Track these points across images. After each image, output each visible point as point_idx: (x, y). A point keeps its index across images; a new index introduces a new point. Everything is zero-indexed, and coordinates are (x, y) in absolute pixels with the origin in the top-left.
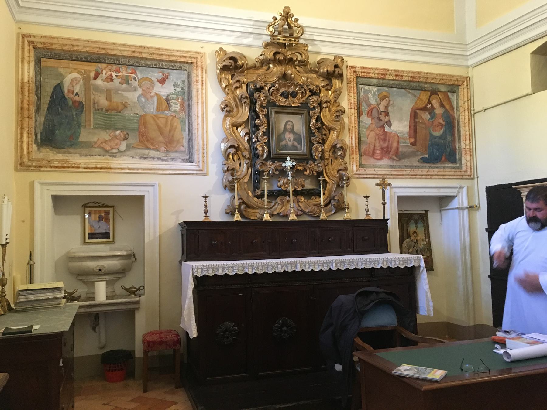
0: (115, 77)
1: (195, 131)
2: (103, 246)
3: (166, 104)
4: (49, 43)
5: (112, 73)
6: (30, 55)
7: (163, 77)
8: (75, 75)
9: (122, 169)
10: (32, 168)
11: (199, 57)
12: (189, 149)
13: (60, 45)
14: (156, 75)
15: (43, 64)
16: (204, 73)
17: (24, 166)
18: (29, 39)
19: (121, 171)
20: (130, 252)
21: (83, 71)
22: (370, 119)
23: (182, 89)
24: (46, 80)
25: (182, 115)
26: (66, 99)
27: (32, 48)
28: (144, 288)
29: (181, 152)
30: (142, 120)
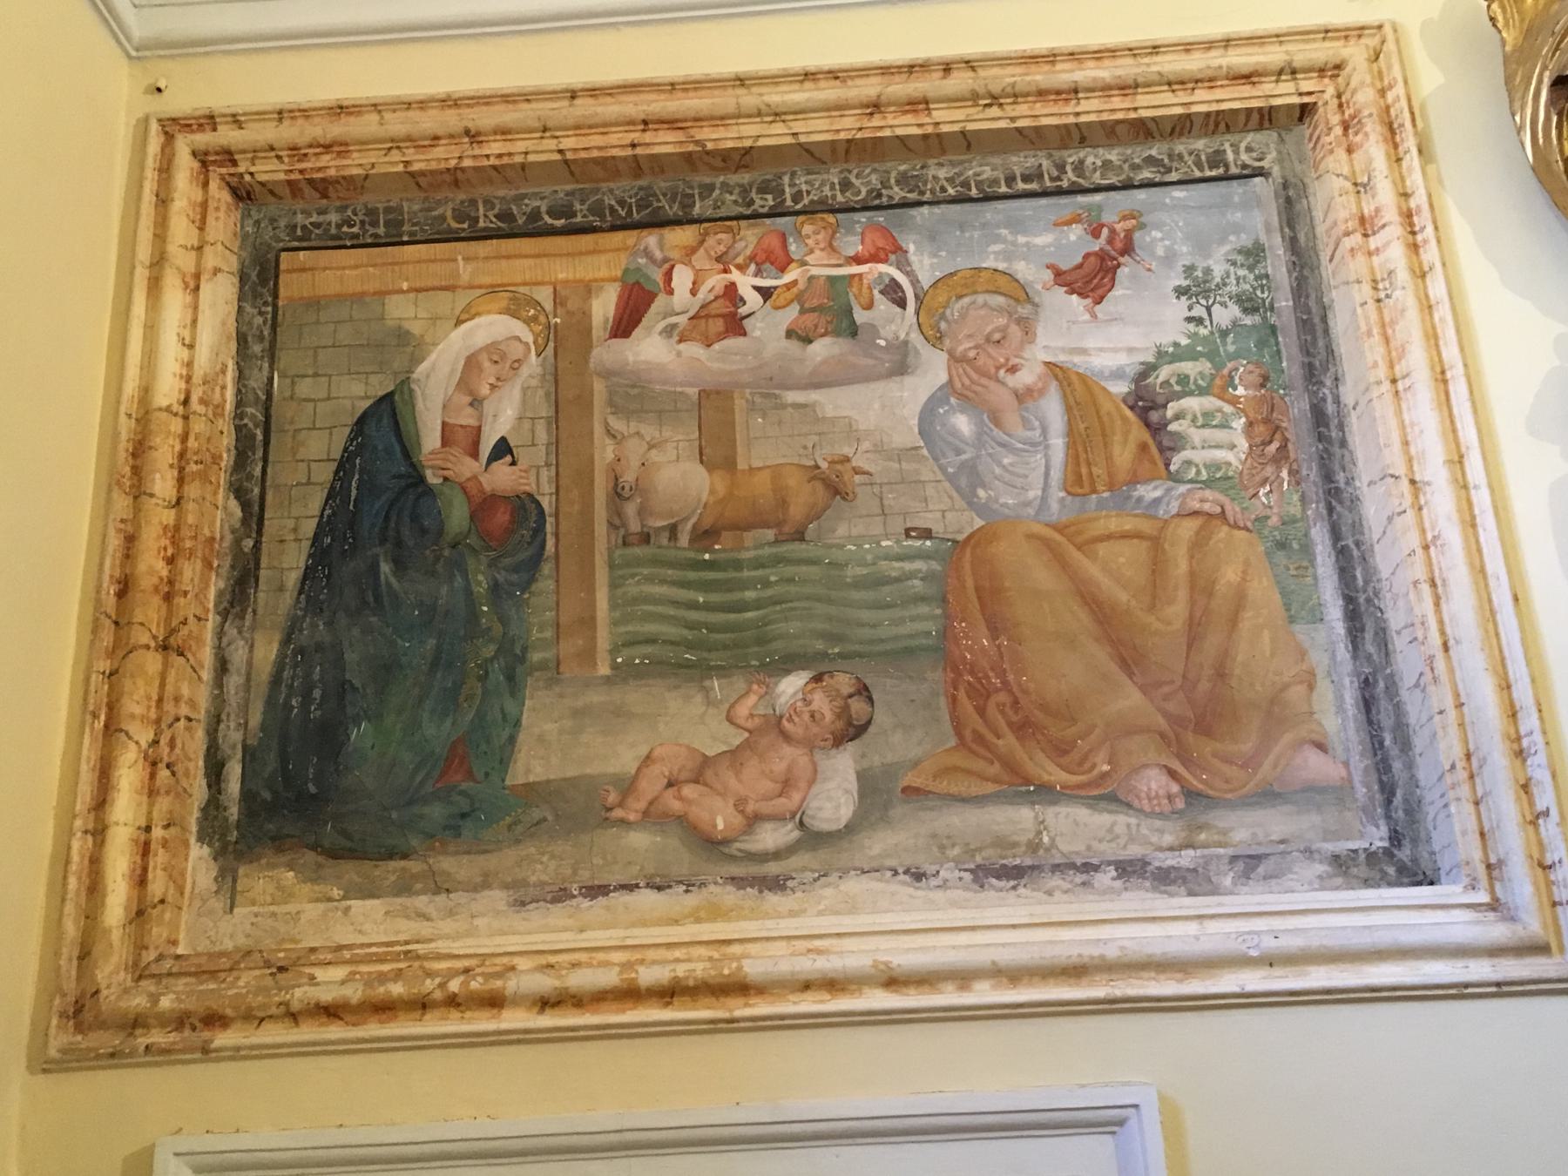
0: (753, 300)
1: (1405, 606)
3: (1139, 433)
4: (327, 147)
5: (735, 276)
6: (213, 240)
7: (1096, 246)
8: (493, 327)
9: (832, 985)
10: (158, 1037)
11: (1355, 54)
12: (1382, 767)
13: (395, 143)
14: (1043, 239)
15: (291, 287)
16: (1412, 160)
17: (102, 1025)
18: (203, 139)
19: (828, 1002)
21: (544, 295)
23: (1249, 304)
24: (305, 388)
25: (1277, 498)
26: (429, 491)
27: (220, 194)
29: (1313, 794)
30: (968, 573)
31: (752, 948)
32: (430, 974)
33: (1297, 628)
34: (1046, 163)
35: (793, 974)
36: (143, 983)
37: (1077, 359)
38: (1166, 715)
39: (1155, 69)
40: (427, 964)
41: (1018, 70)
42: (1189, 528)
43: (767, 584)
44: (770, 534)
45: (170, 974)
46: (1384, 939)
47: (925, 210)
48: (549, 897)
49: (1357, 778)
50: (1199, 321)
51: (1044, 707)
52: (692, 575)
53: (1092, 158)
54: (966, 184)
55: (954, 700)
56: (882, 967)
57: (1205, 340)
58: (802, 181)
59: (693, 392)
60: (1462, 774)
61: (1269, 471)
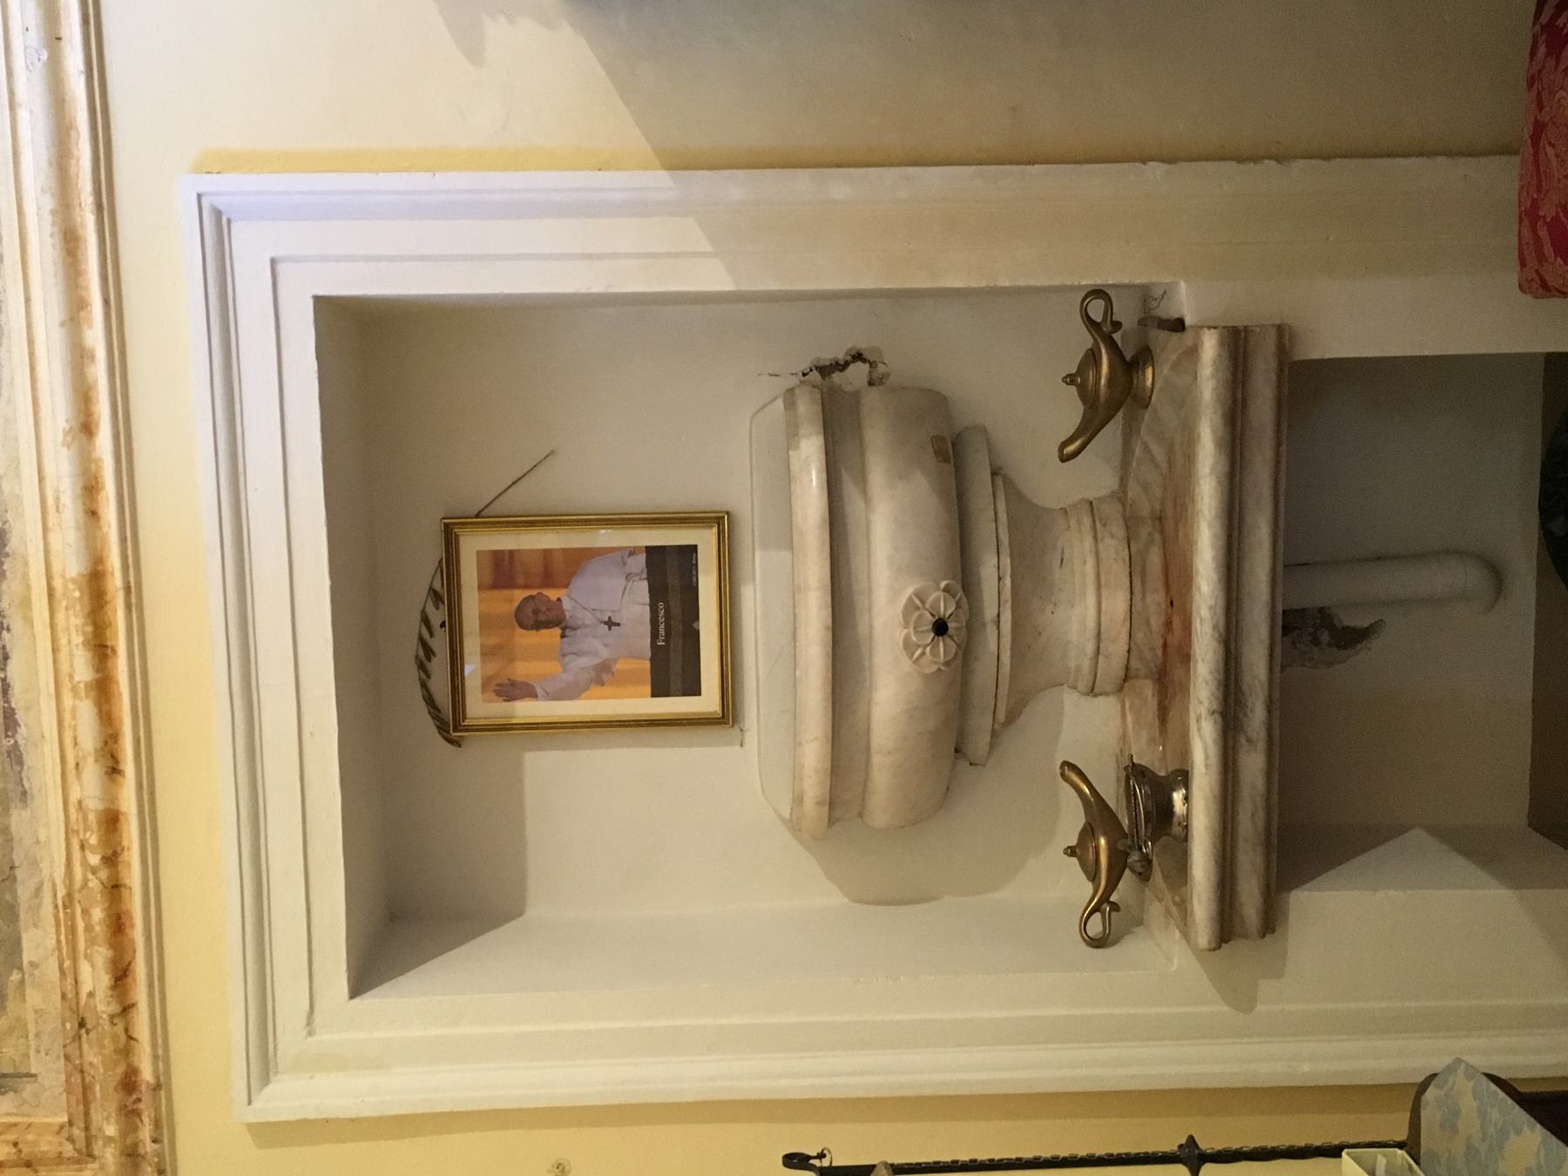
2: (751, 600)
9: (90, 489)
10: (146, 1133)
20: (807, 406)
28: (1098, 293)
32: (86, 881)
35: (78, 529)
36: (96, 1153)
40: (78, 885)
45: (87, 1129)
48: (18, 768)
56: (69, 438)
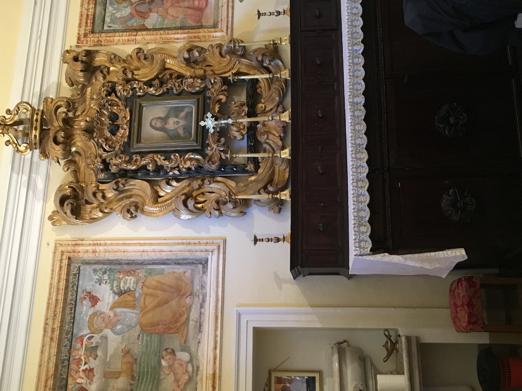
0: (87, 366)
1: (164, 256)
5: (81, 370)
7: (88, 299)
9: (215, 358)
11: (61, 249)
14: (85, 308)
16: (83, 242)
19: (218, 359)
20: (335, 350)
22: (151, 14)
23: (105, 273)
25: (142, 273)
28: (386, 330)
29: (192, 275)
30: (147, 329)
31: (208, 372)
33: (165, 273)
34: (69, 306)
37: (110, 305)
38: (177, 296)
39: (55, 284)
41: (50, 310)
42: (144, 288)
43: (144, 366)
44: (135, 365)
46: (216, 269)
47: (74, 330)
49: (190, 268)
50: (106, 282)
51: (173, 317)
52: (140, 381)
53: (70, 297)
54: (70, 322)
55: (170, 333)
57: (110, 281)
58: (63, 355)
59: (104, 379)
60: (192, 253)
61: (136, 273)
